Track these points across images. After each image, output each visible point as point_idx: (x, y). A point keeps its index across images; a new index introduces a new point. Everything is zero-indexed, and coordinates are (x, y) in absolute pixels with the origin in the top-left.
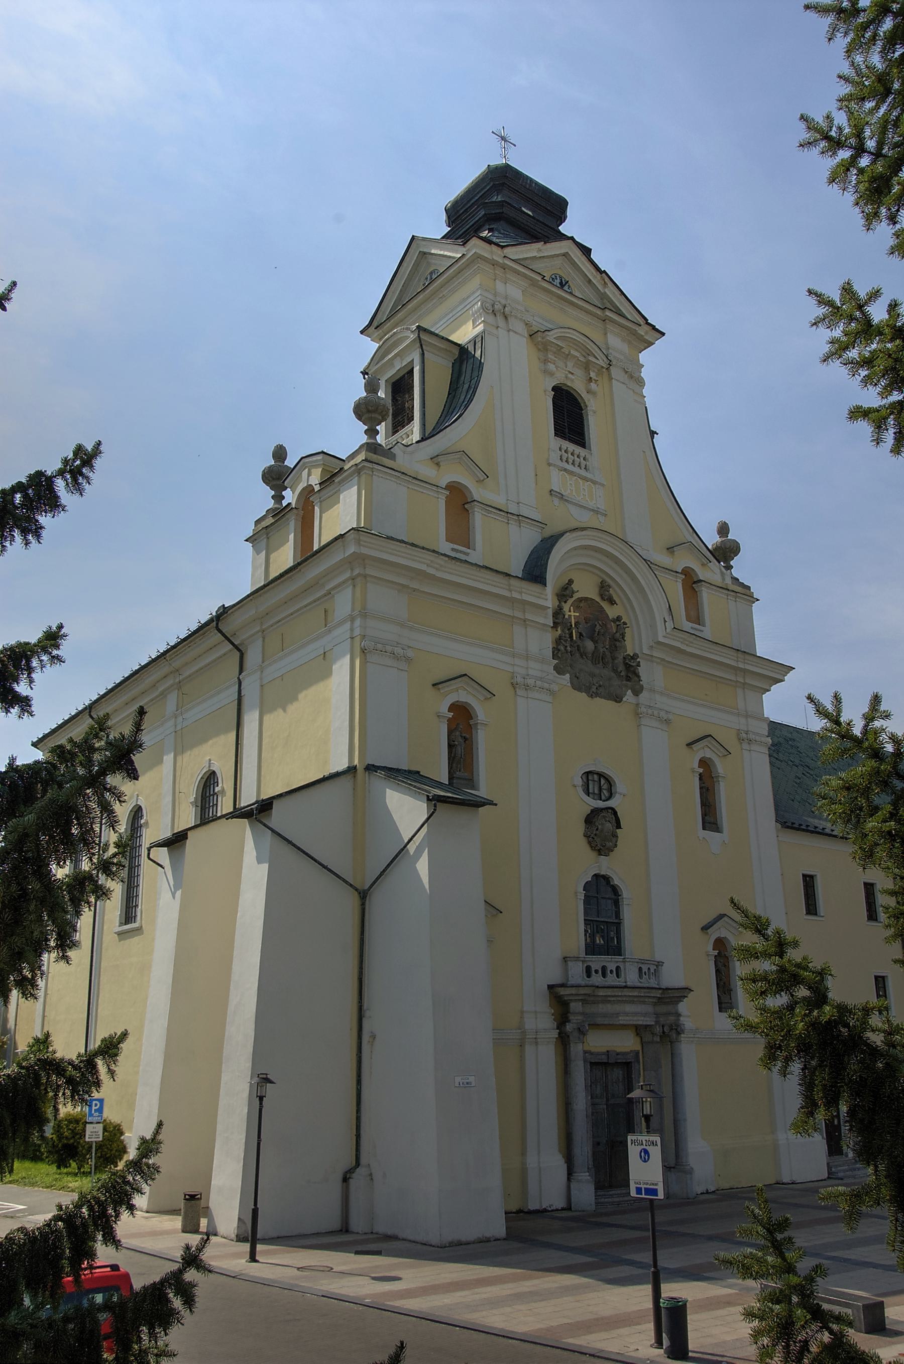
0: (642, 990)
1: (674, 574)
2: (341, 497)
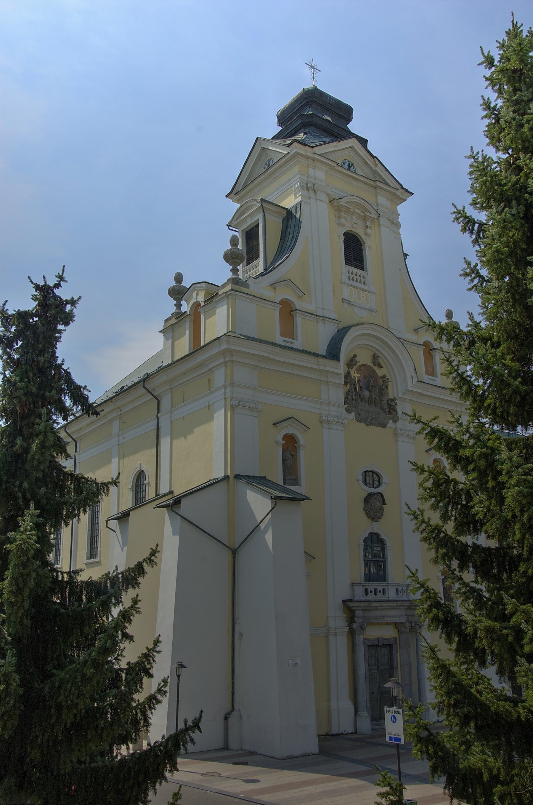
0: (398, 602)
1: (419, 346)
2: (217, 311)
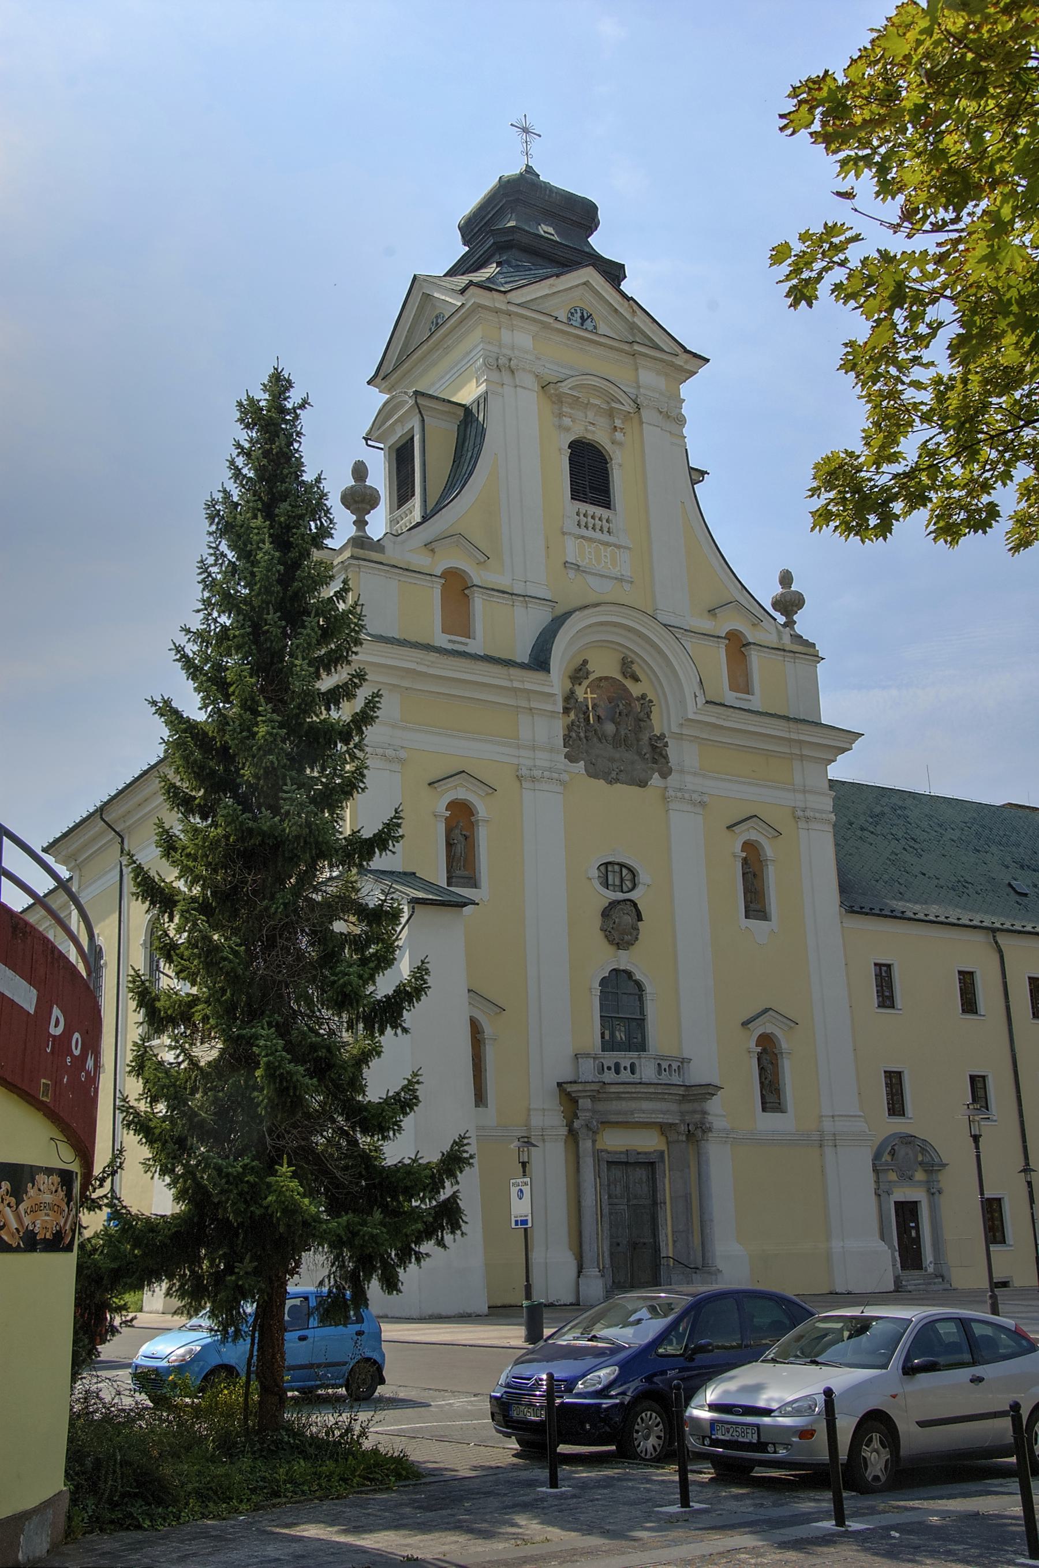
0: (659, 1086)
1: (716, 639)
